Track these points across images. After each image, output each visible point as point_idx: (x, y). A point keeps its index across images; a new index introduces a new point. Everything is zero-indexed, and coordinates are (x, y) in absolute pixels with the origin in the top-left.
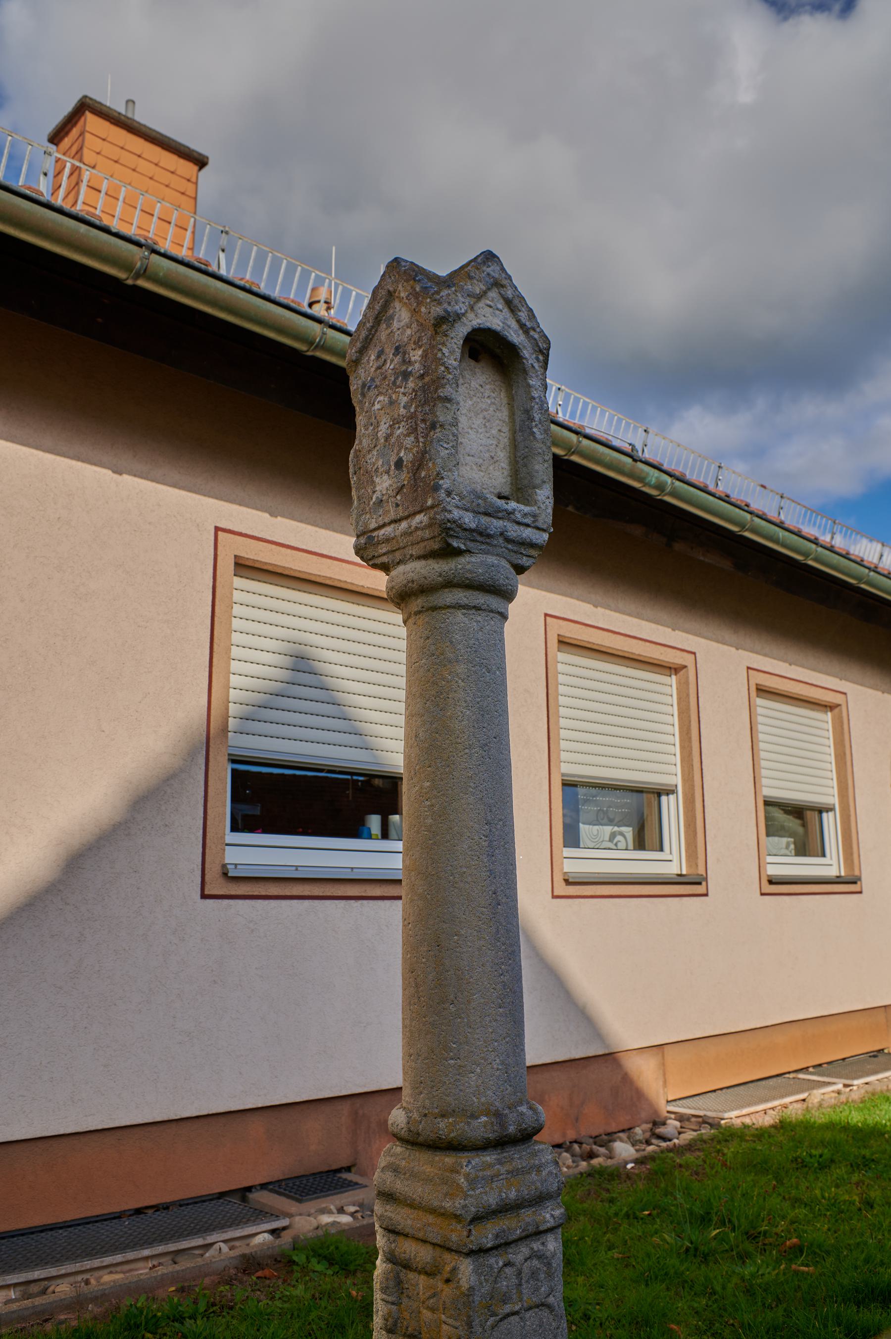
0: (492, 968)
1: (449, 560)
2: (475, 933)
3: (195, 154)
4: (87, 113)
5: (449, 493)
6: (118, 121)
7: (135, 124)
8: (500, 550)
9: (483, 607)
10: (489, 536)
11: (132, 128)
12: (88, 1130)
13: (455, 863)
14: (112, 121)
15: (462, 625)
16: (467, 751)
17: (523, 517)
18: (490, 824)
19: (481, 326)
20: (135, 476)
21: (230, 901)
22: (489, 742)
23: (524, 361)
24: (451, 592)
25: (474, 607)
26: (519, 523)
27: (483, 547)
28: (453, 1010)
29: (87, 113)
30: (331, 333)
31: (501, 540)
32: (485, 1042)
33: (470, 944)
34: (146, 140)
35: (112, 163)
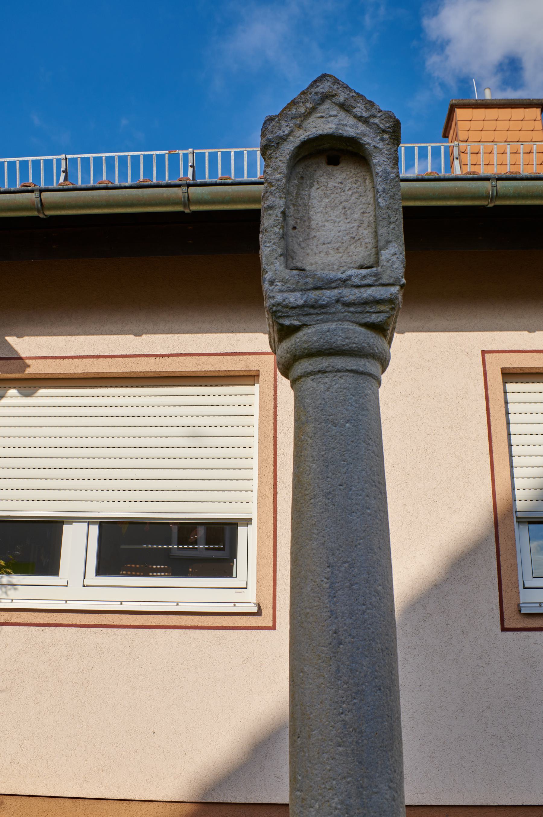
0: (331, 706)
1: (291, 338)
2: (315, 671)
3: (535, 101)
4: (456, 109)
5: (272, 283)
6: (477, 105)
7: (488, 101)
8: (341, 316)
9: (327, 370)
10: (322, 306)
11: (487, 105)
12: (419, 804)
13: (302, 604)
14: (473, 107)
15: (311, 389)
16: (312, 501)
17: (362, 280)
18: (333, 566)
19: (310, 137)
20: (413, 331)
21: (528, 632)
22: (333, 490)
23: (366, 146)
24: (300, 363)
25: (319, 371)
26: (358, 286)
27: (320, 317)
28: (300, 742)
29: (456, 109)
30: (500, 184)
31: (339, 307)
32: (322, 778)
33: (311, 681)
34: (499, 108)
35: (480, 132)
